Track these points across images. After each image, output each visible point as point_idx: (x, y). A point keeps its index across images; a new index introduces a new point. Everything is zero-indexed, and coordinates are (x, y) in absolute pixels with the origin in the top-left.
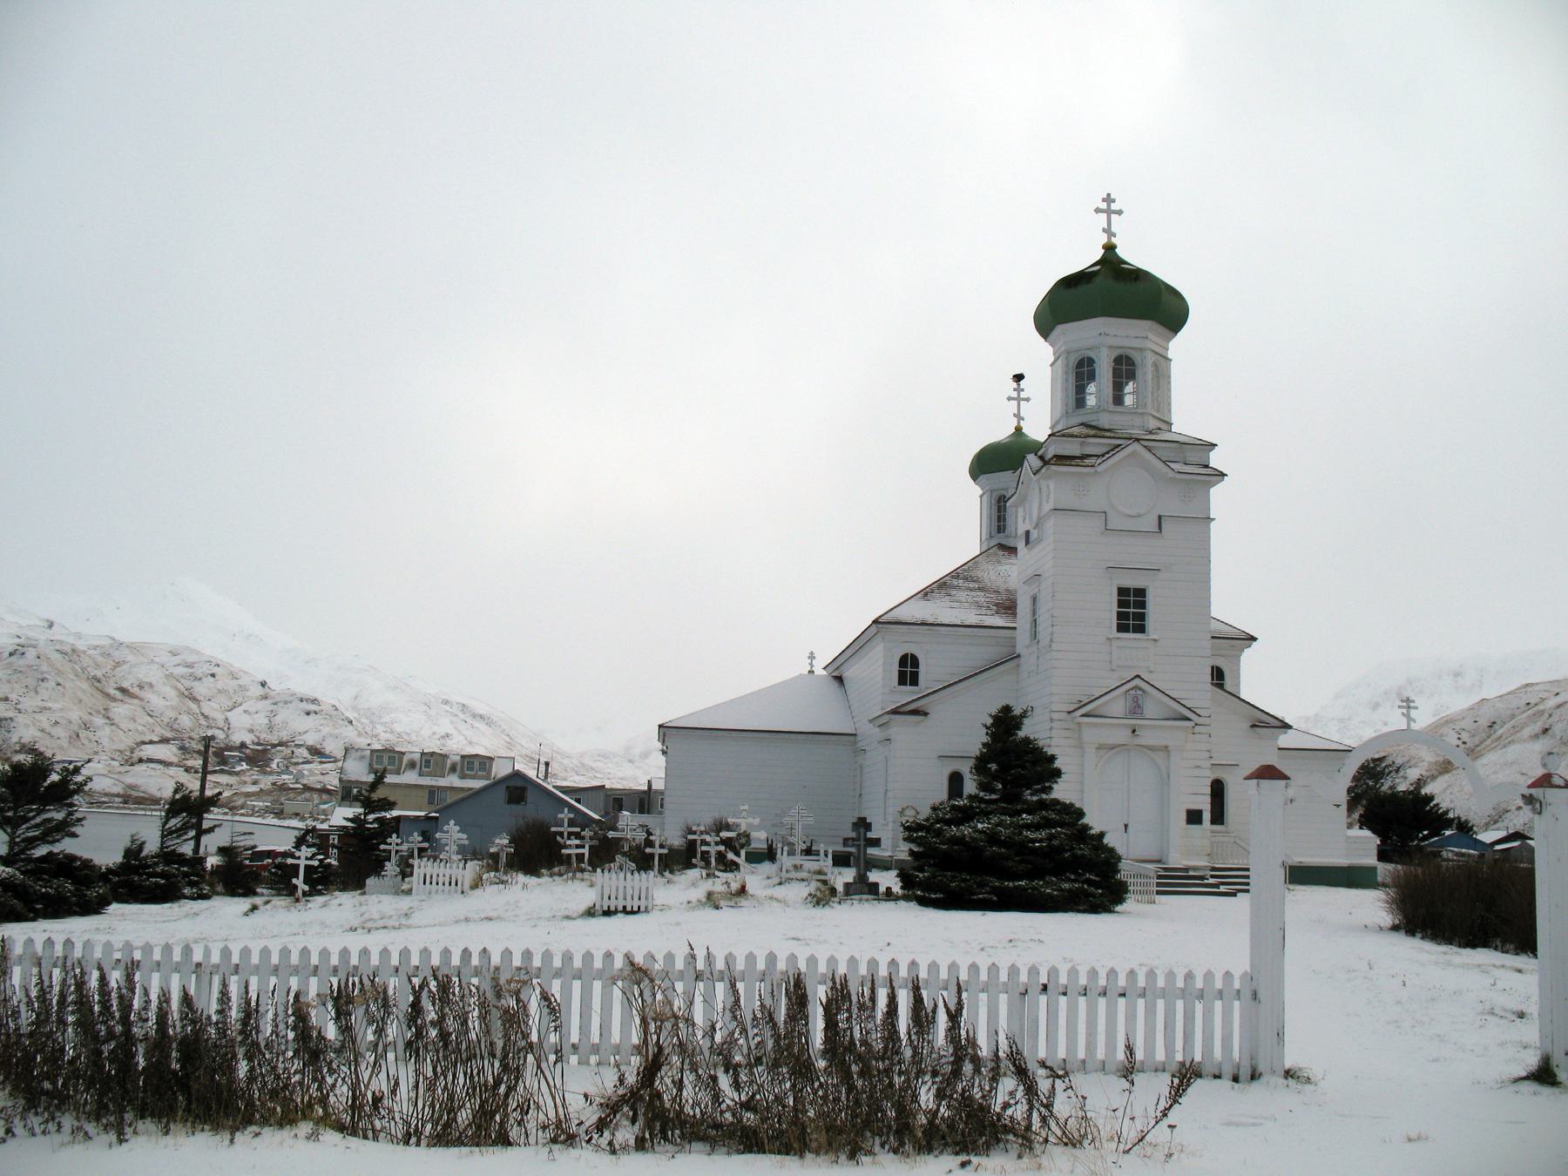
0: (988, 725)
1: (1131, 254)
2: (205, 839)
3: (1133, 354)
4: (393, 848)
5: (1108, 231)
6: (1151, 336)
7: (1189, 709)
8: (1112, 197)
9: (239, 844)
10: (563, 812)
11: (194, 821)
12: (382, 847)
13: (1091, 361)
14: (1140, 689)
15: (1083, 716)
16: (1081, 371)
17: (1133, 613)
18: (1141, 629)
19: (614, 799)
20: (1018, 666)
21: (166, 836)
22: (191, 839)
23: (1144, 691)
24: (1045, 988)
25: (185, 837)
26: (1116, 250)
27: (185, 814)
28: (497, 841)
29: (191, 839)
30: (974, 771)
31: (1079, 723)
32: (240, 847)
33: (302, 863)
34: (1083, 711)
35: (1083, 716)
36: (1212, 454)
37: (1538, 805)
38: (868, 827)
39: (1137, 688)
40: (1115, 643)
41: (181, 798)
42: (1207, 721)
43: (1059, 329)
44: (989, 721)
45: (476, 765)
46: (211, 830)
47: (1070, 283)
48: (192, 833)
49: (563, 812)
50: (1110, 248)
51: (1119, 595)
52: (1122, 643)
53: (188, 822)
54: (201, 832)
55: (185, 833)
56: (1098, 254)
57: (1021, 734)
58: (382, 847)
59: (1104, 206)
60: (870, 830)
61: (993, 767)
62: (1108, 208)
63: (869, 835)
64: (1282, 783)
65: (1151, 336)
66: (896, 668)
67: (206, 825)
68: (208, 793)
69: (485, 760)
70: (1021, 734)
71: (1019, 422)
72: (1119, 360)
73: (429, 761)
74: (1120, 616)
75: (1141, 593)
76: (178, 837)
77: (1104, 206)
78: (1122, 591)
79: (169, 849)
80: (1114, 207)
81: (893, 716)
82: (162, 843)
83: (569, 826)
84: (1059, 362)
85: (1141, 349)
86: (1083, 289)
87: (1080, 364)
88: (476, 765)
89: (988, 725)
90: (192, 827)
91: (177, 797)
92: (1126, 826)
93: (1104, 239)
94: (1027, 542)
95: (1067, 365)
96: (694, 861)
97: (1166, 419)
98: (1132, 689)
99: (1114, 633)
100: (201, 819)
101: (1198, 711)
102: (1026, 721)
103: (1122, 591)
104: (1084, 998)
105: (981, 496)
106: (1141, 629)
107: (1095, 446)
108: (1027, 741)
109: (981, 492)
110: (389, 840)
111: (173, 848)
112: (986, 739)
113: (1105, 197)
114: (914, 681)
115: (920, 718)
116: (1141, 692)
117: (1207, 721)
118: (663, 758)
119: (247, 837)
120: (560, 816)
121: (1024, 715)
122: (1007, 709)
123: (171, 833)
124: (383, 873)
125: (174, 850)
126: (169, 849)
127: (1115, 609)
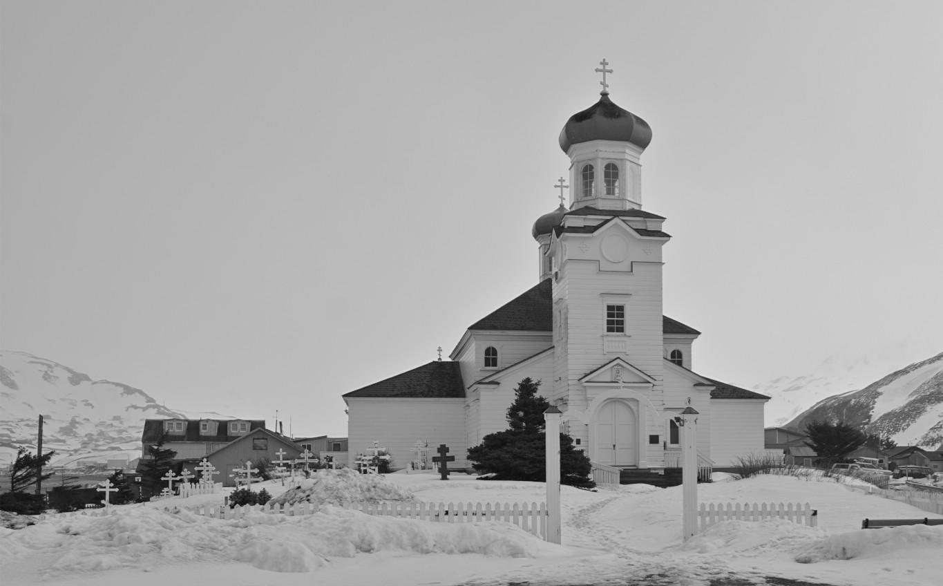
0: (517, 389)
1: (613, 98)
2: (44, 484)
3: (618, 164)
4: (170, 479)
5: (604, 84)
6: (627, 151)
7: (649, 376)
8: (606, 61)
9: (68, 485)
10: (279, 451)
11: (35, 471)
12: (163, 479)
13: (591, 167)
14: (620, 365)
15: (587, 382)
16: (587, 174)
17: (617, 321)
18: (621, 330)
19: (335, 445)
20: (554, 353)
21: (15, 482)
22: (34, 483)
23: (623, 367)
24: (447, 513)
25: (29, 482)
26: (609, 96)
27: (28, 467)
28: (234, 470)
29: (34, 483)
30: (508, 416)
31: (585, 387)
32: (68, 487)
33: (107, 491)
34: (587, 379)
35: (587, 382)
36: (663, 224)
37: (682, 422)
38: (447, 450)
39: (618, 365)
40: (605, 339)
41: (24, 457)
42: (660, 383)
43: (573, 147)
44: (517, 387)
45: (239, 427)
46: (47, 477)
47: (579, 118)
48: (35, 479)
49: (283, 451)
50: (604, 95)
51: (608, 310)
52: (609, 339)
53: (30, 472)
54: (41, 479)
55: (29, 480)
56: (597, 99)
57: (537, 395)
58: (163, 479)
59: (601, 67)
60: (448, 452)
61: (521, 414)
62: (604, 69)
63: (448, 454)
64: (559, 414)
65: (627, 151)
66: (483, 356)
67: (43, 474)
68: (43, 453)
69: (236, 423)
70: (537, 395)
71: (562, 201)
72: (608, 167)
73: (206, 425)
74: (609, 322)
75: (621, 308)
76: (24, 482)
77: (601, 67)
78: (610, 308)
79: (18, 491)
80: (607, 68)
81: (478, 386)
82: (13, 487)
83: (283, 460)
84: (573, 168)
85: (621, 160)
86: (586, 123)
87: (585, 169)
88: (239, 427)
89: (517, 389)
90: (33, 476)
91: (22, 456)
92: (614, 446)
93: (601, 89)
94: (556, 278)
95: (578, 170)
96: (103, 502)
97: (638, 202)
98: (616, 365)
99: (606, 333)
100: (40, 471)
101: (654, 378)
102: (539, 387)
103: (610, 308)
104: (466, 517)
105: (540, 248)
106: (621, 330)
107: (592, 221)
108: (541, 399)
109: (539, 246)
110: (167, 474)
111: (20, 490)
112: (516, 398)
113: (606, 61)
114: (495, 364)
115: (496, 386)
116: (620, 367)
117: (660, 383)
118: (347, 416)
119: (74, 480)
120: (278, 453)
121: (519, 384)
122: (528, 380)
123: (19, 480)
124: (161, 494)
125: (22, 491)
126: (18, 491)
127: (606, 318)
